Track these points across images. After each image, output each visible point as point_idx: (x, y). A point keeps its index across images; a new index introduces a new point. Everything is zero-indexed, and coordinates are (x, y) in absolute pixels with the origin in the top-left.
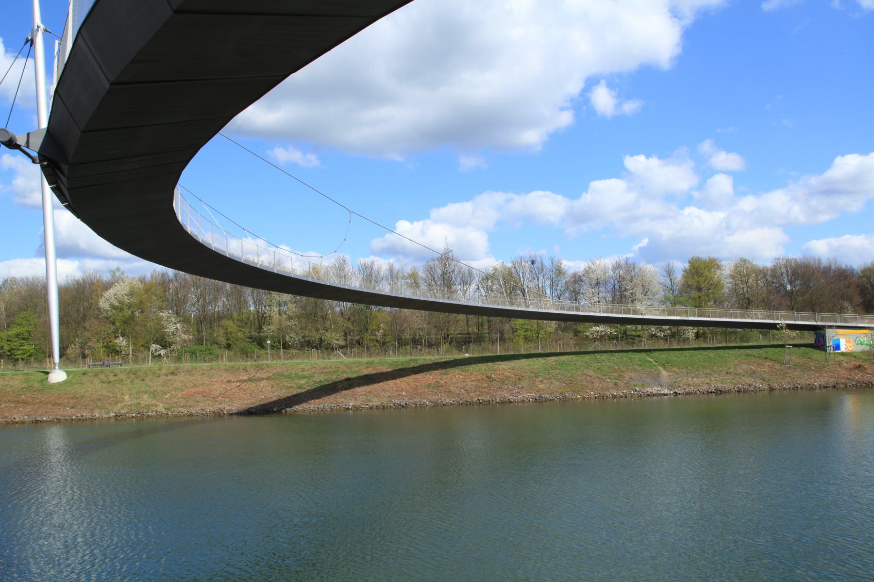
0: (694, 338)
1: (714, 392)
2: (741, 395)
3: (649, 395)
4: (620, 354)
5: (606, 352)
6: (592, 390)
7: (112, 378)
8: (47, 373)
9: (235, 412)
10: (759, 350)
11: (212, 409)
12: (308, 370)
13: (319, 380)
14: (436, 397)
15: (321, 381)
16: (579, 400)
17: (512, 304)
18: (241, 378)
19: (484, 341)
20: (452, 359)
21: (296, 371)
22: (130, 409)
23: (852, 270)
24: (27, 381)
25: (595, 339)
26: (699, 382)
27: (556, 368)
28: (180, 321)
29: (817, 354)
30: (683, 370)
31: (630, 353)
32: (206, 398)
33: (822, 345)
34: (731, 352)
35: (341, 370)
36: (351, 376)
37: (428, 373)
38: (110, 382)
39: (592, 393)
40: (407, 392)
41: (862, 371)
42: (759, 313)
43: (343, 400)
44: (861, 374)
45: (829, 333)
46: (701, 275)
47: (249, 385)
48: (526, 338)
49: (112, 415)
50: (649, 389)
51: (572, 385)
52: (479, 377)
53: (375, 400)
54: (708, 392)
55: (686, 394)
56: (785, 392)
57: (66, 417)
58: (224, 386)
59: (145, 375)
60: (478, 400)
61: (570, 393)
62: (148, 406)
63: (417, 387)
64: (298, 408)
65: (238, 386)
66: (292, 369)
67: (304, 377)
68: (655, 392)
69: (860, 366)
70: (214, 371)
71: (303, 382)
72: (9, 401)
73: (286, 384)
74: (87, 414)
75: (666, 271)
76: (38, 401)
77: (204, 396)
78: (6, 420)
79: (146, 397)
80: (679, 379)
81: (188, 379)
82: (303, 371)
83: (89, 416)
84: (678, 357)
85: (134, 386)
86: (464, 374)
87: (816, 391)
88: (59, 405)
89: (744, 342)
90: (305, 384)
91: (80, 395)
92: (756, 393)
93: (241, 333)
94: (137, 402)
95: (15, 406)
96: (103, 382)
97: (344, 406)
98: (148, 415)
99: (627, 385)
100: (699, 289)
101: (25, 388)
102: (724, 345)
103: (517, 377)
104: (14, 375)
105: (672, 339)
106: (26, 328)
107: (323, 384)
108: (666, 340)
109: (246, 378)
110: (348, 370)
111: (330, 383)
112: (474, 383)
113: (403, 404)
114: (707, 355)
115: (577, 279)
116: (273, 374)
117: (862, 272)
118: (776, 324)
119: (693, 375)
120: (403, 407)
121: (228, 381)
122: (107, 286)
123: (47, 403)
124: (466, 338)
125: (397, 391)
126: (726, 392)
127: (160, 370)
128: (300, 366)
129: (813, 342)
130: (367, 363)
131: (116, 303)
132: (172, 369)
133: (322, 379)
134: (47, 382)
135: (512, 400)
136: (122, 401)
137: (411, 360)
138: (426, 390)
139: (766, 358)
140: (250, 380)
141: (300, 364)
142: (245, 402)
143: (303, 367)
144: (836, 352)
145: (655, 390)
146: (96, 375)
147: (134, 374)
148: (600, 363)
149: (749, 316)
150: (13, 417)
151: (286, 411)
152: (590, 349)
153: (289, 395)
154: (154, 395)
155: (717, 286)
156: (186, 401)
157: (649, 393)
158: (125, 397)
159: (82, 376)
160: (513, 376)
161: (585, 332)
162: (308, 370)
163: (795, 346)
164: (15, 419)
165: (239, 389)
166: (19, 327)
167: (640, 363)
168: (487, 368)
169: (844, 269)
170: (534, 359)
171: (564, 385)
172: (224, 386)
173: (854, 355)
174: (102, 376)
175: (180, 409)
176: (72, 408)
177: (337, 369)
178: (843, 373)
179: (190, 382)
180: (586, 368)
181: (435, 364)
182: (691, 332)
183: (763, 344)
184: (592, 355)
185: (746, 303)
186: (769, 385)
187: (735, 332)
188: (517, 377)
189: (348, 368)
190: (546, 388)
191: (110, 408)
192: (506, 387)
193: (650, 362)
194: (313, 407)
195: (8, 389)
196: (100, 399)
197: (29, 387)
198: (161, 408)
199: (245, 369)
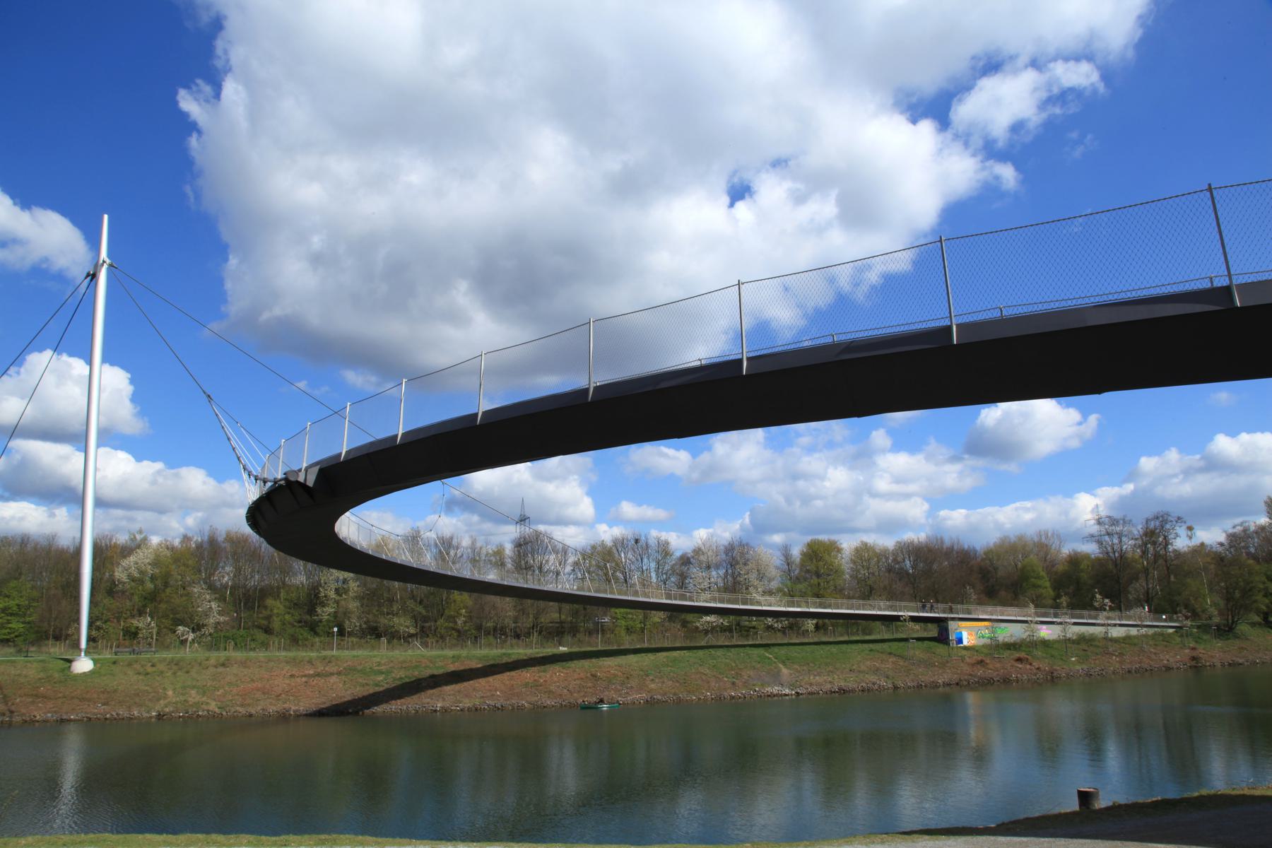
0: (813, 630)
1: (837, 692)
2: (866, 693)
4: (737, 649)
5: (721, 647)
6: (707, 691)
7: (150, 670)
8: (70, 661)
9: (304, 713)
10: (882, 644)
11: (275, 709)
12: (385, 665)
13: (398, 676)
14: (536, 698)
15: (401, 678)
16: (694, 702)
18: (307, 672)
19: (578, 631)
20: (550, 654)
21: (371, 665)
22: (176, 707)
23: (975, 551)
25: (706, 632)
26: (822, 681)
27: (668, 666)
28: (216, 599)
29: (940, 649)
30: (805, 668)
31: (748, 648)
34: (854, 647)
35: (424, 665)
36: (436, 672)
37: (525, 670)
38: (147, 674)
39: (708, 694)
40: (501, 691)
41: (984, 666)
43: (429, 700)
44: (983, 669)
45: (952, 625)
46: (821, 559)
47: (315, 681)
48: (628, 629)
49: (154, 714)
50: (769, 689)
51: (686, 684)
52: (582, 675)
53: (467, 700)
54: (831, 692)
55: (808, 694)
56: (909, 690)
57: (99, 716)
58: (287, 682)
59: (189, 666)
60: (583, 701)
61: (685, 694)
62: (197, 704)
63: (513, 686)
64: (378, 709)
66: (366, 662)
67: (381, 673)
68: (775, 692)
69: (982, 661)
70: (273, 663)
71: (381, 678)
72: (25, 695)
73: (361, 681)
74: (123, 712)
75: (783, 555)
76: (60, 695)
77: (264, 693)
78: (24, 718)
79: (193, 692)
80: (801, 678)
81: (242, 672)
82: (378, 665)
83: (126, 715)
84: (799, 653)
85: (178, 679)
86: (565, 671)
87: (940, 689)
88: (89, 700)
89: (867, 634)
90: (382, 681)
91: (112, 688)
92: (880, 692)
93: (290, 615)
94: (183, 699)
96: (139, 674)
97: (431, 708)
98: (198, 715)
99: (745, 684)
100: (818, 575)
101: (43, 679)
102: (845, 638)
104: (27, 662)
105: (790, 631)
106: (17, 602)
107: (404, 681)
108: (784, 633)
109: (311, 672)
110: (431, 665)
111: (412, 680)
112: (578, 682)
113: (499, 705)
114: (829, 650)
115: (685, 561)
116: (344, 669)
117: (986, 553)
118: (899, 616)
119: (816, 673)
120: (499, 709)
122: (126, 551)
123: (72, 698)
124: (558, 627)
125: (490, 691)
126: (849, 691)
127: (207, 660)
128: (374, 659)
129: (936, 635)
130: (453, 657)
131: (136, 575)
132: (222, 660)
133: (401, 675)
135: (621, 702)
136: (164, 697)
137: (504, 654)
139: (890, 654)
140: (318, 675)
141: (375, 656)
142: (313, 701)
143: (378, 660)
144: (959, 645)
146: (130, 665)
147: (176, 664)
148: (715, 659)
149: (829, 606)
150: (33, 714)
151: (363, 713)
152: (703, 643)
153: (366, 693)
154: (203, 691)
155: (838, 572)
156: (243, 699)
157: (769, 693)
158: (168, 693)
160: (620, 674)
161: (695, 622)
162: (385, 665)
163: (918, 639)
164: (35, 717)
166: (6, 599)
167: (758, 659)
168: (591, 665)
169: (967, 551)
170: (643, 655)
171: (678, 685)
172: (287, 682)
173: (977, 649)
174: (137, 666)
175: (238, 708)
176: (104, 704)
177: (418, 664)
178: (966, 669)
179: (245, 676)
180: (701, 665)
181: (531, 659)
184: (707, 651)
185: (868, 592)
186: (893, 683)
187: (857, 623)
188: (625, 675)
189: (432, 663)
190: (658, 688)
191: (150, 704)
192: (613, 687)
193: (769, 658)
194: (395, 709)
195: (22, 680)
196: (138, 695)
197: (48, 677)
198: (213, 706)
199: (310, 662)
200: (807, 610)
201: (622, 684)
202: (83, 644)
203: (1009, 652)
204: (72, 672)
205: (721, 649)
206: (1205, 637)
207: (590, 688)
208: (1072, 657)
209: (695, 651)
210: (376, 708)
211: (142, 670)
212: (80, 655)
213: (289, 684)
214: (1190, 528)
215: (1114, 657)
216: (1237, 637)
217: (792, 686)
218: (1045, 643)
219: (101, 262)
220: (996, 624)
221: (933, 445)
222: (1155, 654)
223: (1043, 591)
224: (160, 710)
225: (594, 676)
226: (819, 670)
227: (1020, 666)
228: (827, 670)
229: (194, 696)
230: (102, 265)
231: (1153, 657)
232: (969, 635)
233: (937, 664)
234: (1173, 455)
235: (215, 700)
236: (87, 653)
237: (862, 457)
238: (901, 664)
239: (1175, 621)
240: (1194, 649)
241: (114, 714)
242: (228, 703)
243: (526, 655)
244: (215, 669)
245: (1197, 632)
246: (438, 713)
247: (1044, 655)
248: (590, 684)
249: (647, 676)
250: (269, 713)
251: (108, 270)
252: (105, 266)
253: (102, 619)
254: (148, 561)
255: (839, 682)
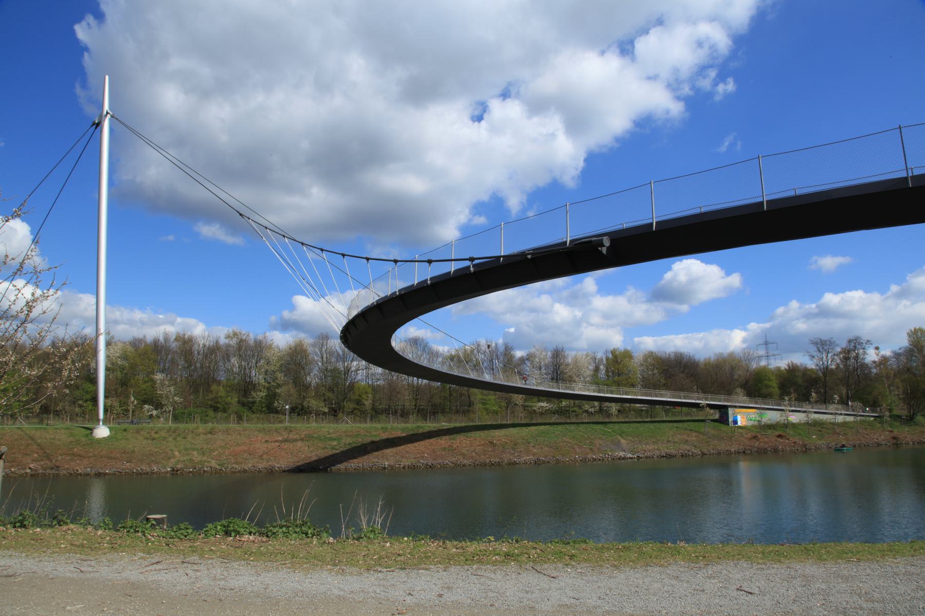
3: (619, 459)
7: (156, 436)
8: (91, 430)
9: (287, 469)
15: (350, 444)
17: (508, 382)
18: (277, 439)
20: (452, 427)
24: (72, 435)
25: (542, 414)
26: (650, 448)
29: (723, 427)
32: (252, 456)
33: (725, 421)
41: (758, 440)
42: (668, 393)
44: (758, 442)
45: (730, 411)
47: (287, 445)
53: (404, 460)
60: (490, 461)
64: (342, 466)
65: (279, 446)
71: (335, 443)
72: (64, 454)
74: (146, 468)
76: (90, 455)
77: (250, 454)
78: (69, 471)
79: (195, 453)
81: (227, 438)
83: (148, 470)
95: (72, 459)
96: (148, 439)
101: (73, 442)
103: (513, 443)
118: (699, 404)
121: (266, 441)
130: (382, 428)
133: (347, 442)
134: (92, 436)
138: (443, 453)
140: (286, 441)
141: (323, 427)
145: (622, 454)
149: (662, 396)
151: (331, 470)
153: (327, 455)
159: (123, 432)
160: (509, 442)
164: (78, 471)
165: (280, 449)
172: (265, 445)
173: (749, 428)
175: (233, 466)
181: (440, 430)
182: (614, 408)
183: (665, 419)
184: (563, 426)
186: (701, 451)
193: (609, 432)
198: (214, 463)
199: (276, 430)
200: (635, 397)
201: (513, 449)
202: (101, 416)
203: (770, 431)
204: (94, 437)
205: (573, 425)
206: (896, 424)
207: (491, 451)
208: (813, 435)
209: (555, 426)
210: (339, 465)
211: (148, 436)
212: (99, 424)
213: (267, 448)
214: (877, 348)
215: (841, 436)
216: (916, 424)
217: (631, 452)
218: (794, 426)
219: (105, 113)
220: (763, 411)
221: (631, 291)
222: (867, 434)
223: (773, 390)
224: (174, 467)
225: (491, 443)
226: (646, 441)
227: (781, 441)
228: (652, 441)
229: (196, 456)
230: (106, 116)
231: (866, 436)
232: (743, 418)
233: (725, 438)
234: (794, 304)
235: (213, 459)
236: (105, 422)
237: (573, 300)
238: (702, 437)
239: (876, 413)
240: (891, 431)
241: (139, 469)
242: (225, 461)
243: (435, 427)
244: (205, 436)
245: (890, 420)
246: (386, 470)
247: (795, 433)
248: (490, 449)
249: (529, 443)
250: (259, 469)
251: (110, 120)
252: (109, 116)
253: (82, 399)
254: (118, 355)
255: (665, 449)
